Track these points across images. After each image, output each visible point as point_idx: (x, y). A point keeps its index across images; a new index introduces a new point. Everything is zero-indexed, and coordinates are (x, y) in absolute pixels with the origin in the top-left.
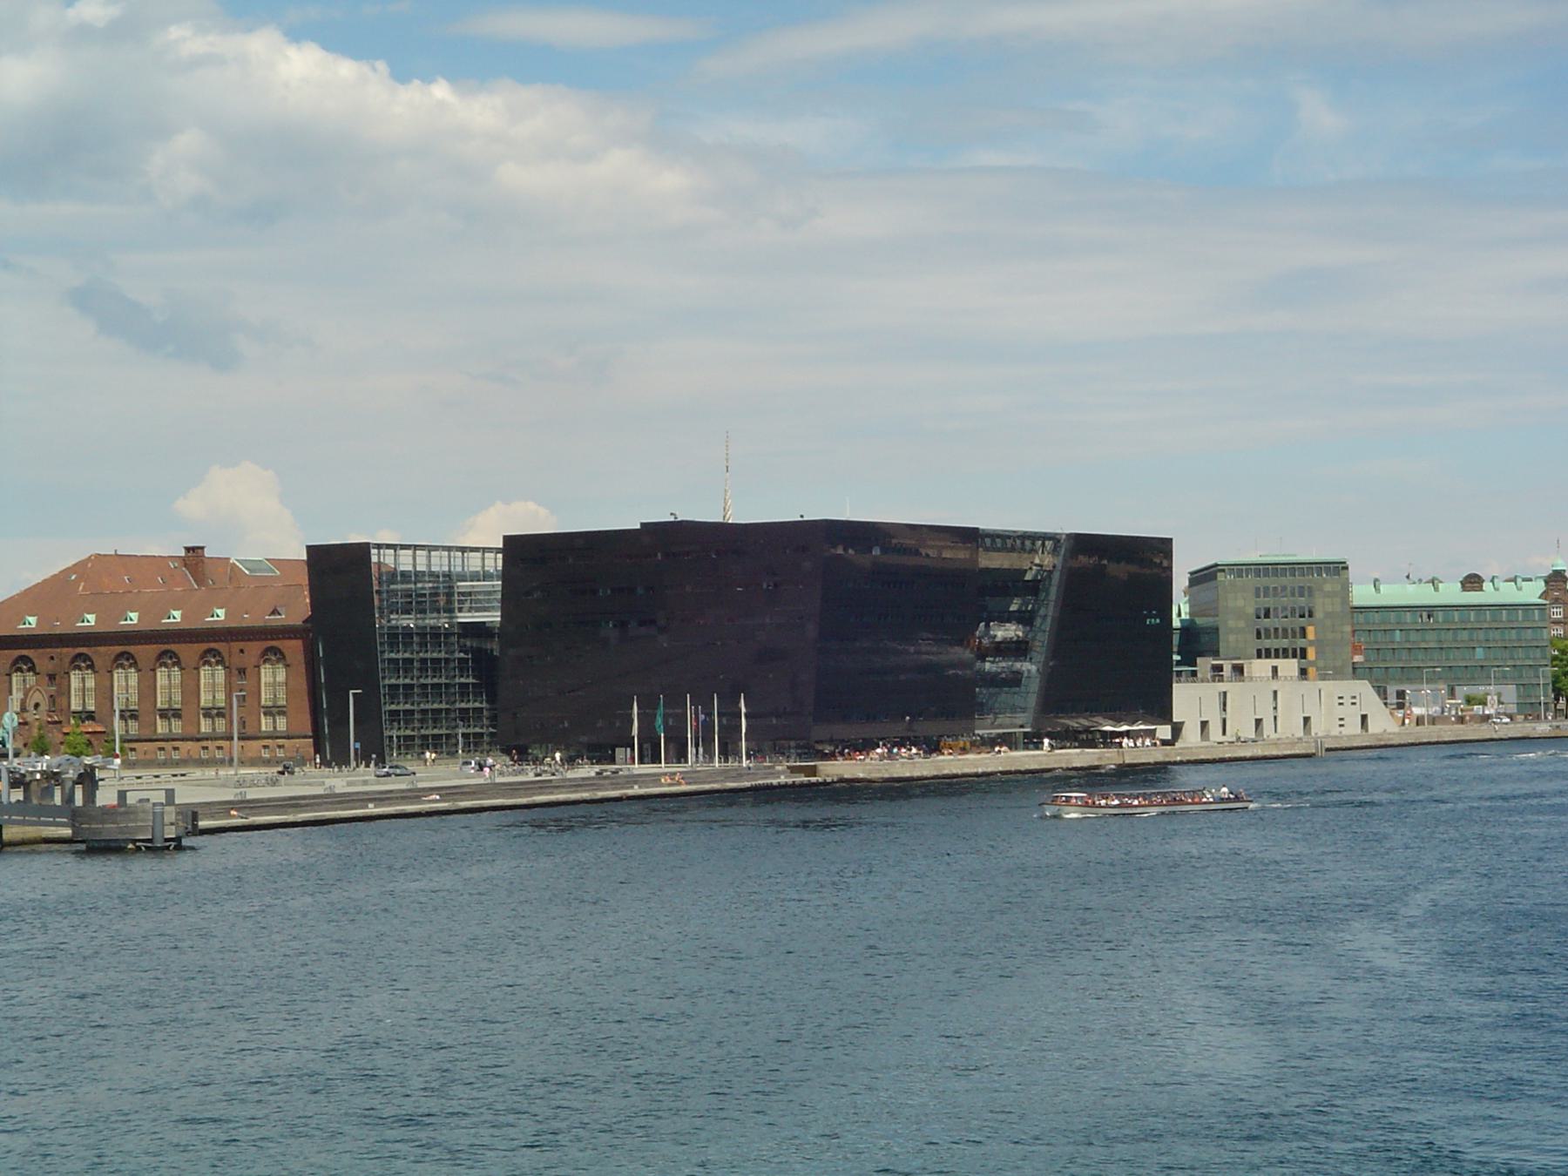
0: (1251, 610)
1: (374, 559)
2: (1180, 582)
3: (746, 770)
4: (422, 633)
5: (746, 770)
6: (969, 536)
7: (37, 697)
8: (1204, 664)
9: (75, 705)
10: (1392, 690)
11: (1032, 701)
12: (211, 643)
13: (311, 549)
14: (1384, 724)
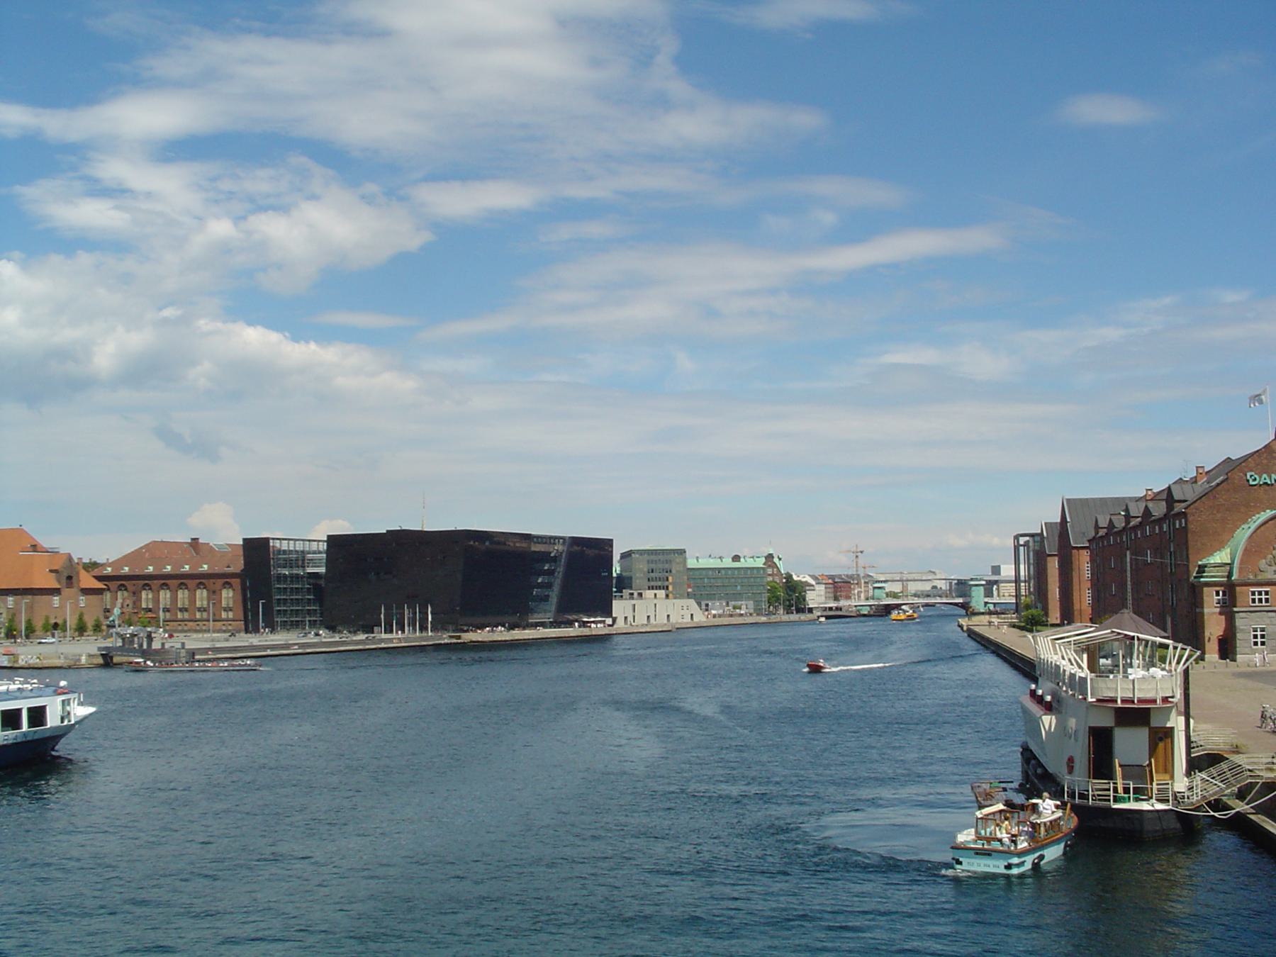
2: (616, 557)
3: (430, 637)
4: (292, 576)
5: (430, 637)
6: (527, 537)
7: (128, 602)
8: (626, 592)
9: (144, 606)
10: (703, 603)
11: (553, 608)
12: (201, 580)
13: (244, 540)
14: (700, 618)
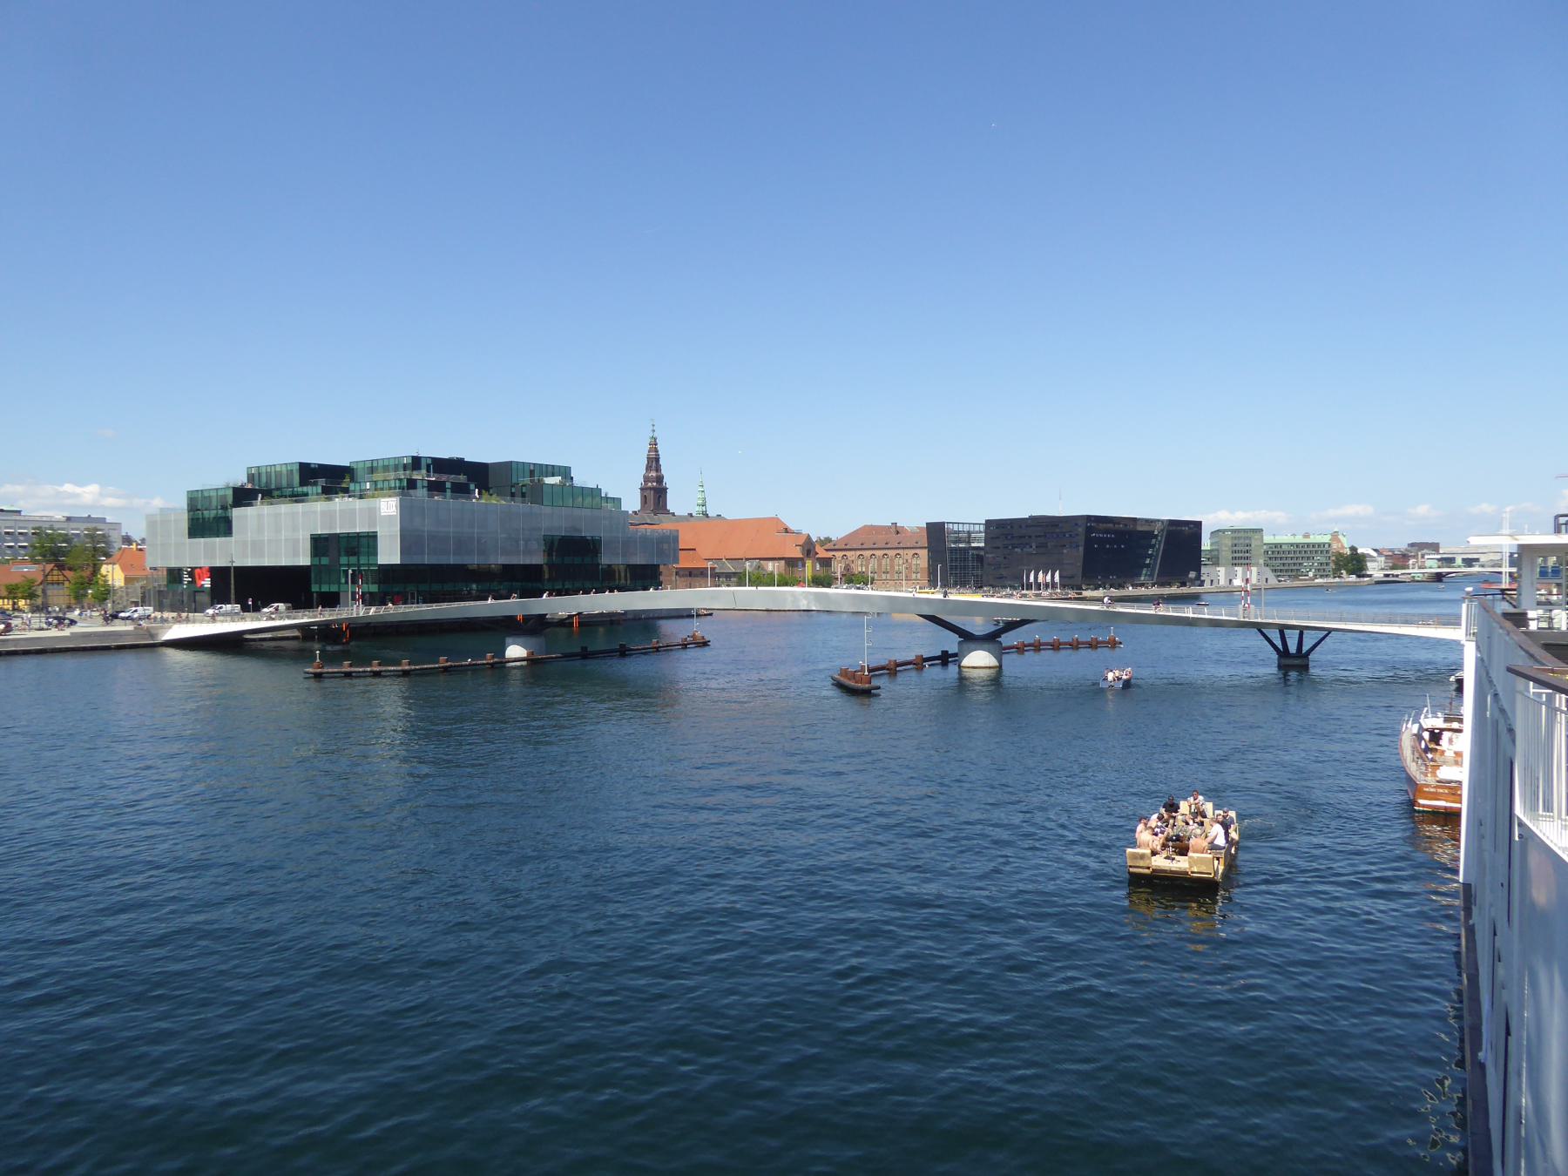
6: (1135, 520)
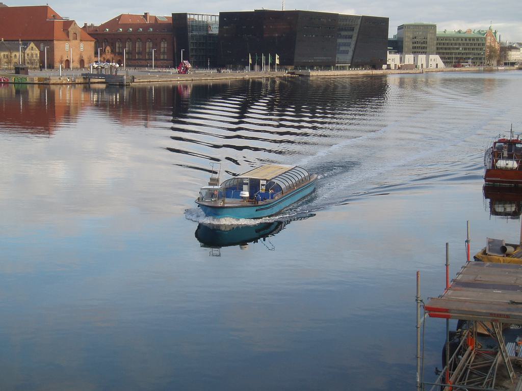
0: (411, 37)
1: (188, 17)
